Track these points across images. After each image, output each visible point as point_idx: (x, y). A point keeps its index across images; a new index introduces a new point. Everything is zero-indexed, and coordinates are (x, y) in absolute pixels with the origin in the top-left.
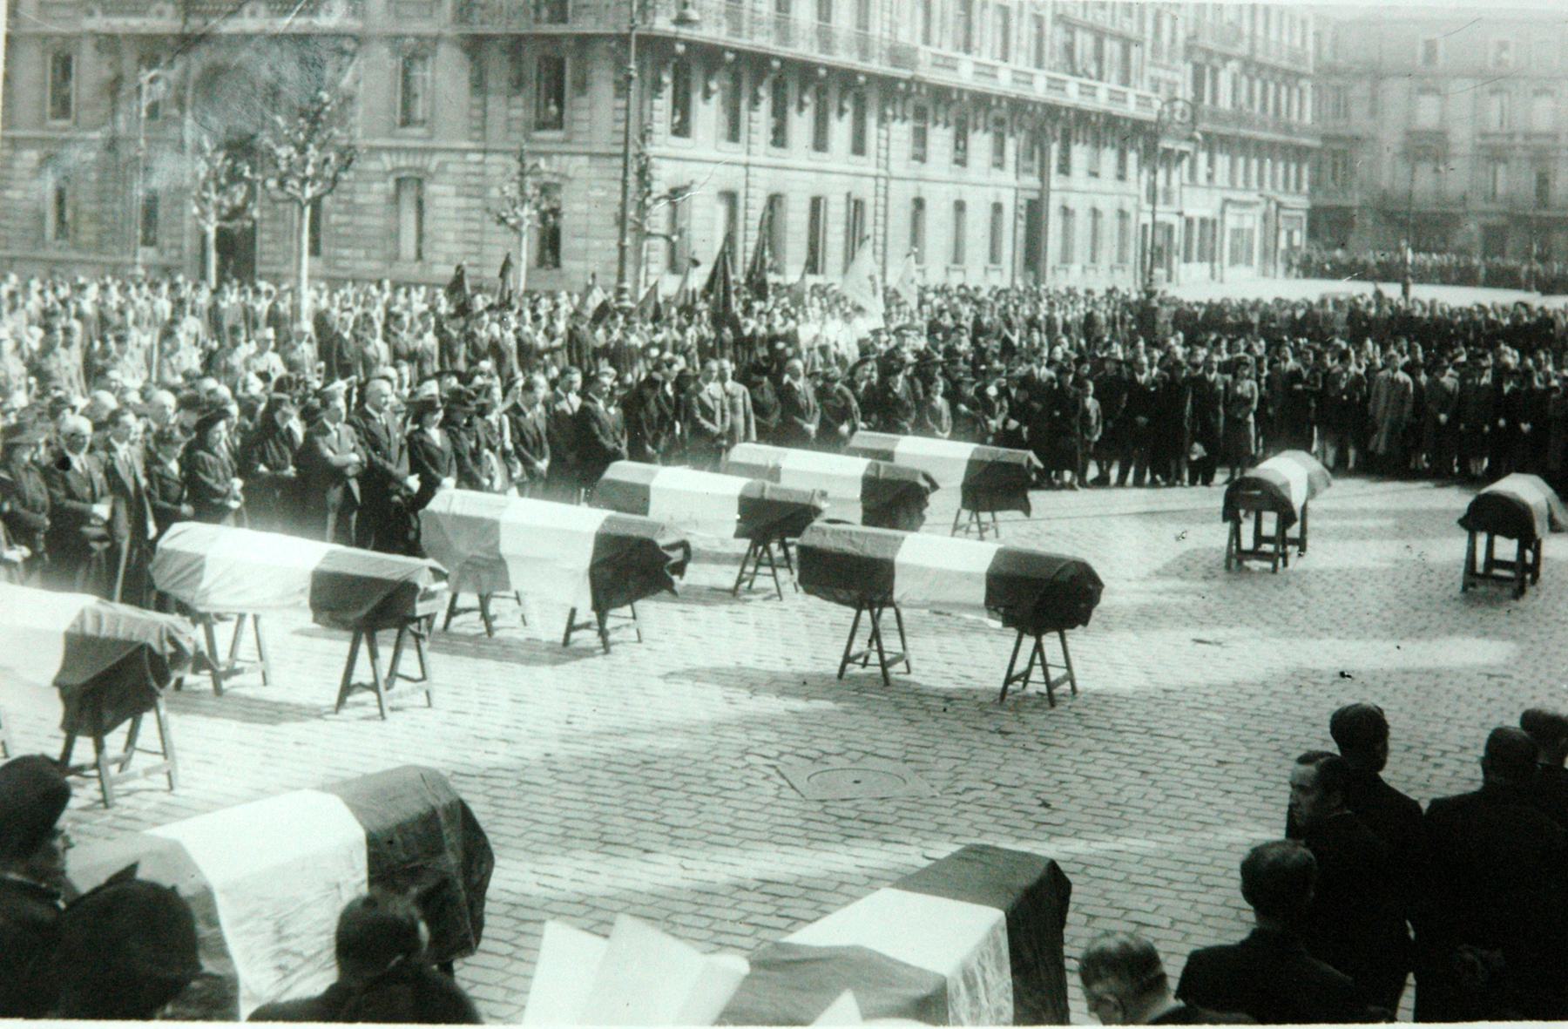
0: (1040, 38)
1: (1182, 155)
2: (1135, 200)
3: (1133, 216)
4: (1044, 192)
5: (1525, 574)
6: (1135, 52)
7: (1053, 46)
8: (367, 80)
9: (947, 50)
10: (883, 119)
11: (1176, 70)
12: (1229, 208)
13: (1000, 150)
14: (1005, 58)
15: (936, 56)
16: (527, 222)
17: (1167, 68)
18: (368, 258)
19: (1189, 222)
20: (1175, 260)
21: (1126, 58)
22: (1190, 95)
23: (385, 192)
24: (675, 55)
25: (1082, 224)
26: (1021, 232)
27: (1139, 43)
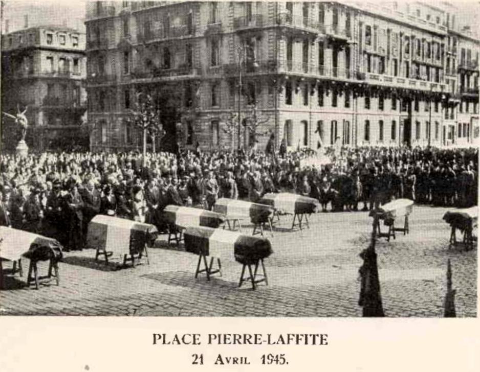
0: (408, 67)
1: (457, 103)
2: (440, 118)
3: (440, 123)
4: (410, 116)
5: (468, 245)
6: (440, 72)
7: (412, 70)
8: (202, 94)
9: (376, 74)
10: (355, 97)
11: (455, 76)
12: (474, 120)
13: (394, 104)
14: (396, 74)
15: (371, 75)
16: (233, 132)
17: (451, 76)
18: (204, 145)
19: (460, 125)
20: (455, 136)
21: (437, 73)
22: (460, 84)
23: (208, 125)
24: (286, 79)
25: (423, 127)
26: (402, 129)
27: (442, 68)
